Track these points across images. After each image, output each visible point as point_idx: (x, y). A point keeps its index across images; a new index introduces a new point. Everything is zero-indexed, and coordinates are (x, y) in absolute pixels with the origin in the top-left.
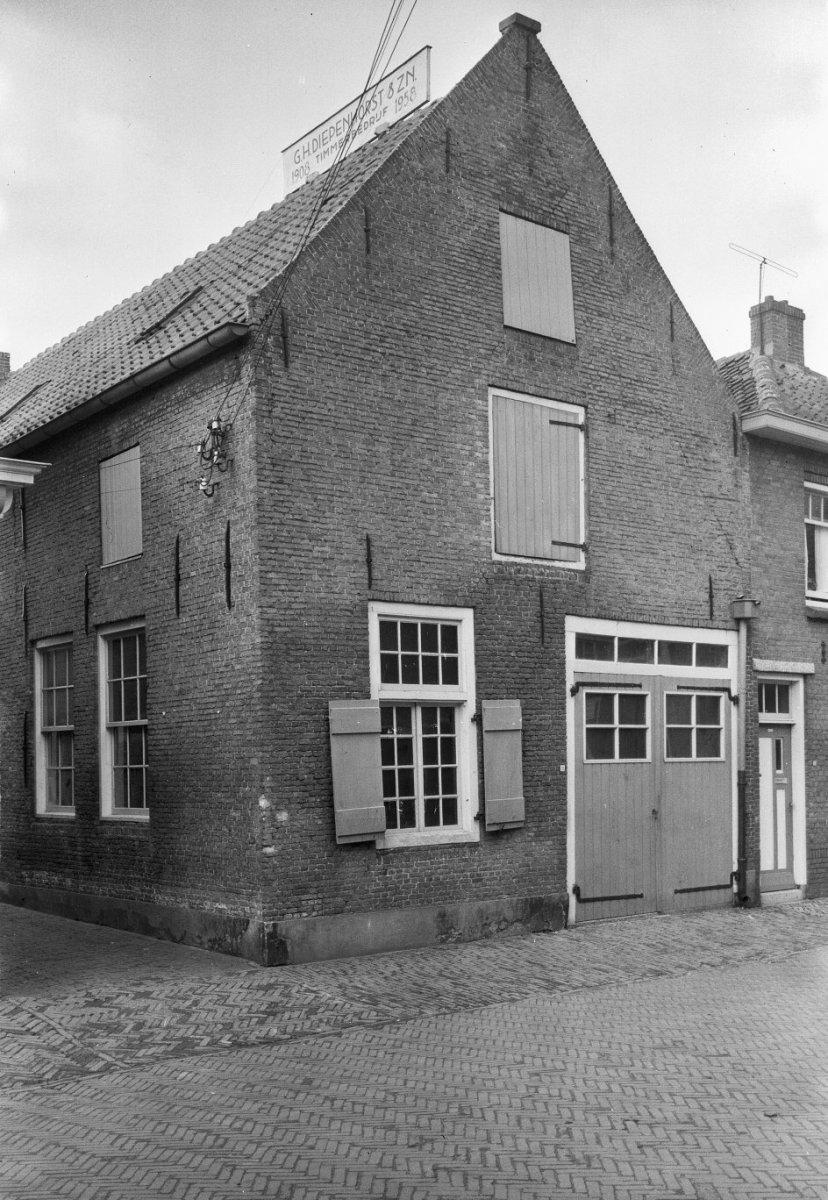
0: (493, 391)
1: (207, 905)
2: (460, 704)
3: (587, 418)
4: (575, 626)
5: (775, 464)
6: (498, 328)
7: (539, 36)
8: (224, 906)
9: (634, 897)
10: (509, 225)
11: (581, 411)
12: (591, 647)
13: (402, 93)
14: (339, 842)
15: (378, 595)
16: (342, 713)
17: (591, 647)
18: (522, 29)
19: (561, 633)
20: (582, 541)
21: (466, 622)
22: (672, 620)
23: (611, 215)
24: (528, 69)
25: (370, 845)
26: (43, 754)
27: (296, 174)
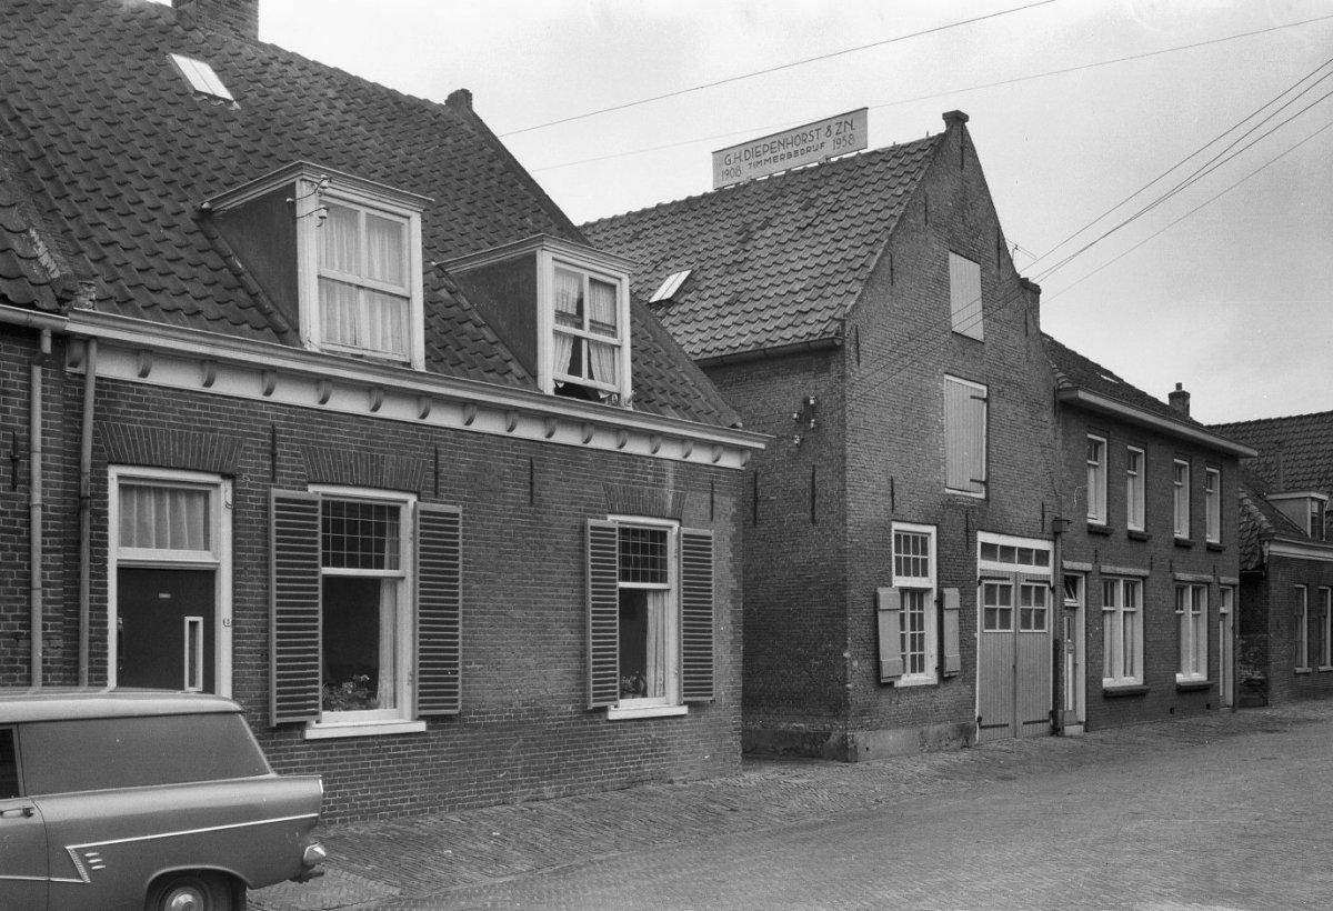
0: (947, 377)
1: (783, 726)
2: (928, 590)
3: (988, 394)
4: (983, 537)
5: (1074, 421)
6: (949, 334)
7: (966, 124)
8: (802, 725)
9: (1028, 723)
10: (953, 257)
11: (985, 388)
12: (989, 550)
13: (840, 136)
14: (883, 681)
15: (897, 517)
16: (882, 592)
17: (989, 550)
18: (956, 120)
19: (975, 542)
20: (984, 479)
21: (932, 530)
22: (1026, 534)
23: (999, 249)
24: (962, 148)
25: (891, 684)
26: (728, 618)
27: (727, 173)
